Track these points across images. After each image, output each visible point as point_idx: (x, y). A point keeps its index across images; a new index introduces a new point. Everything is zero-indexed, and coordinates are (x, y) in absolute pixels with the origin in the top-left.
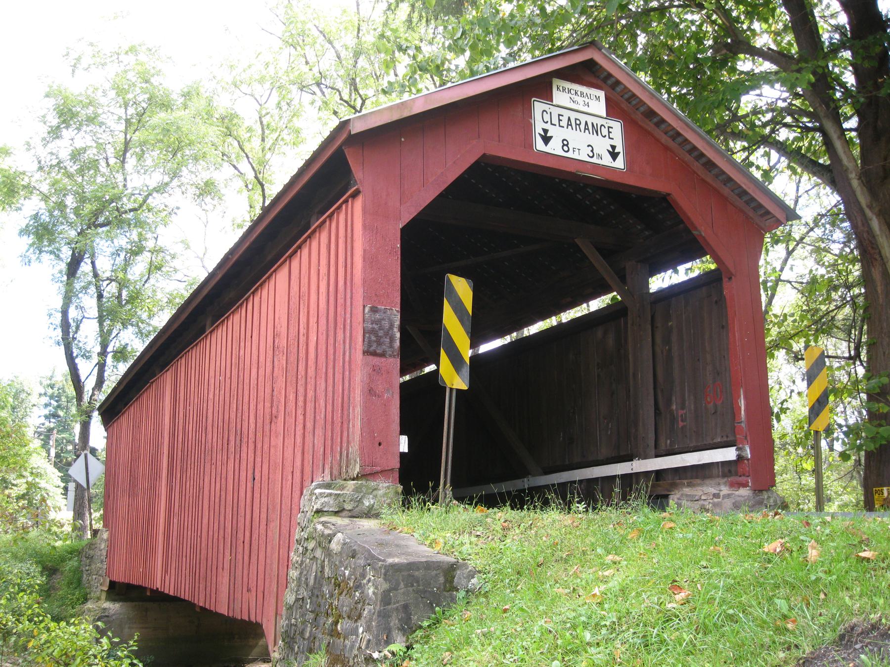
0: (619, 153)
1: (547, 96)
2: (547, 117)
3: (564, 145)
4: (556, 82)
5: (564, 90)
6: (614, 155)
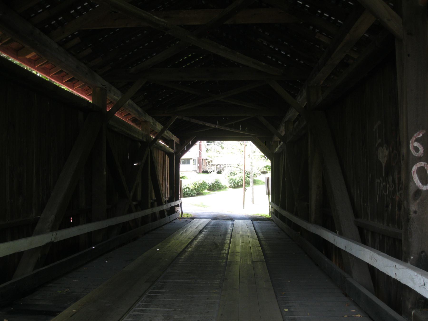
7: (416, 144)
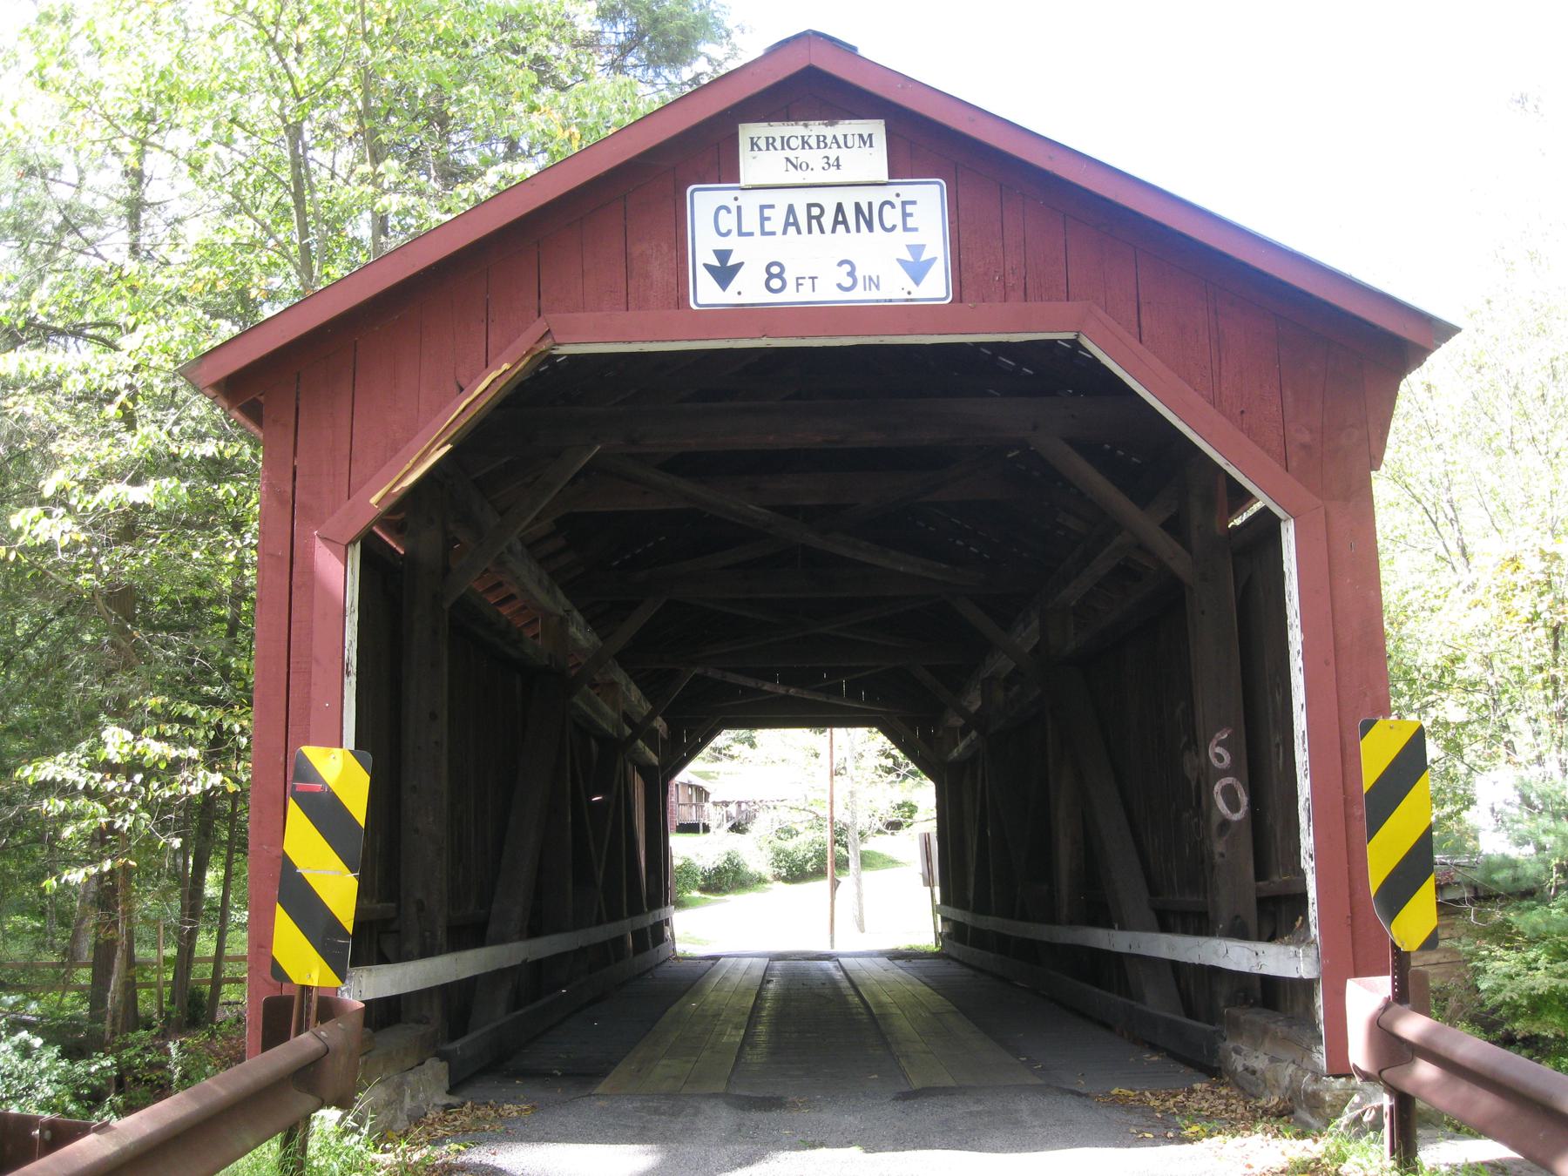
0: (931, 262)
1: (724, 169)
2: (728, 221)
3: (771, 276)
4: (747, 132)
5: (770, 143)
6: (917, 270)
7: (1219, 750)
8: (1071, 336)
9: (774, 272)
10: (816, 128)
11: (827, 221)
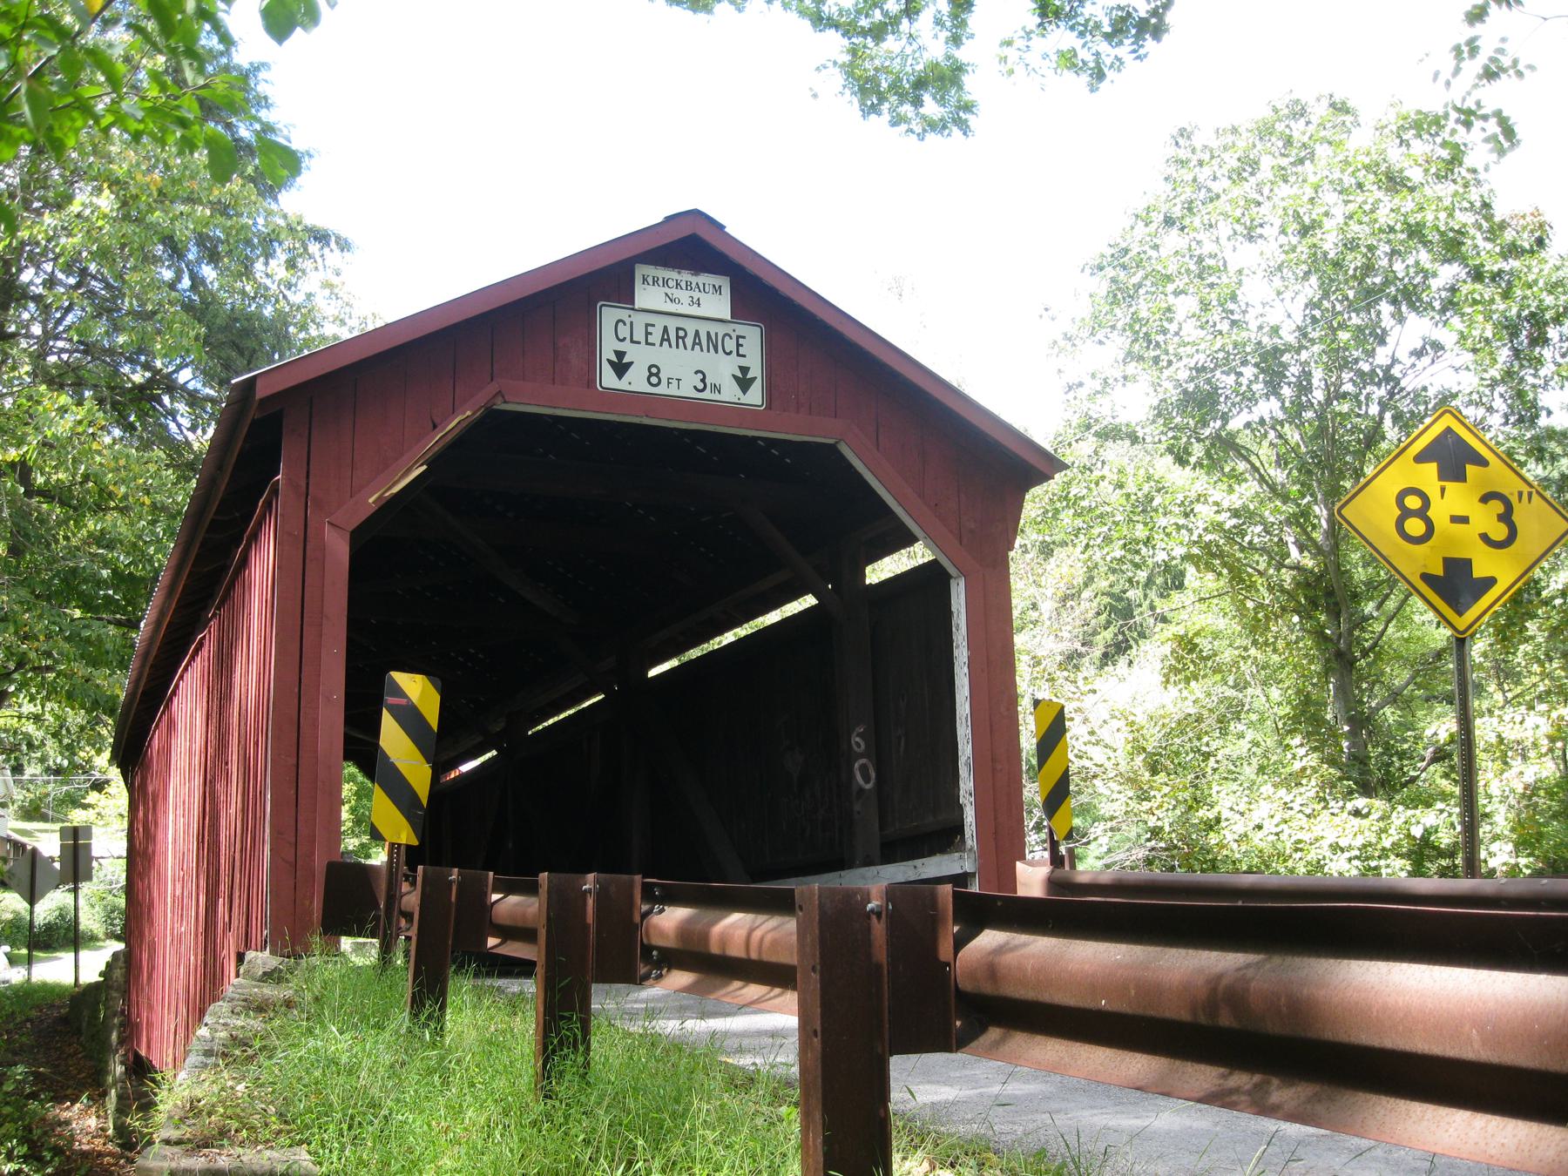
2: (624, 331)
3: (651, 374)
4: (641, 270)
6: (744, 383)
8: (831, 441)
9: (654, 372)
10: (686, 276)
11: (689, 341)
